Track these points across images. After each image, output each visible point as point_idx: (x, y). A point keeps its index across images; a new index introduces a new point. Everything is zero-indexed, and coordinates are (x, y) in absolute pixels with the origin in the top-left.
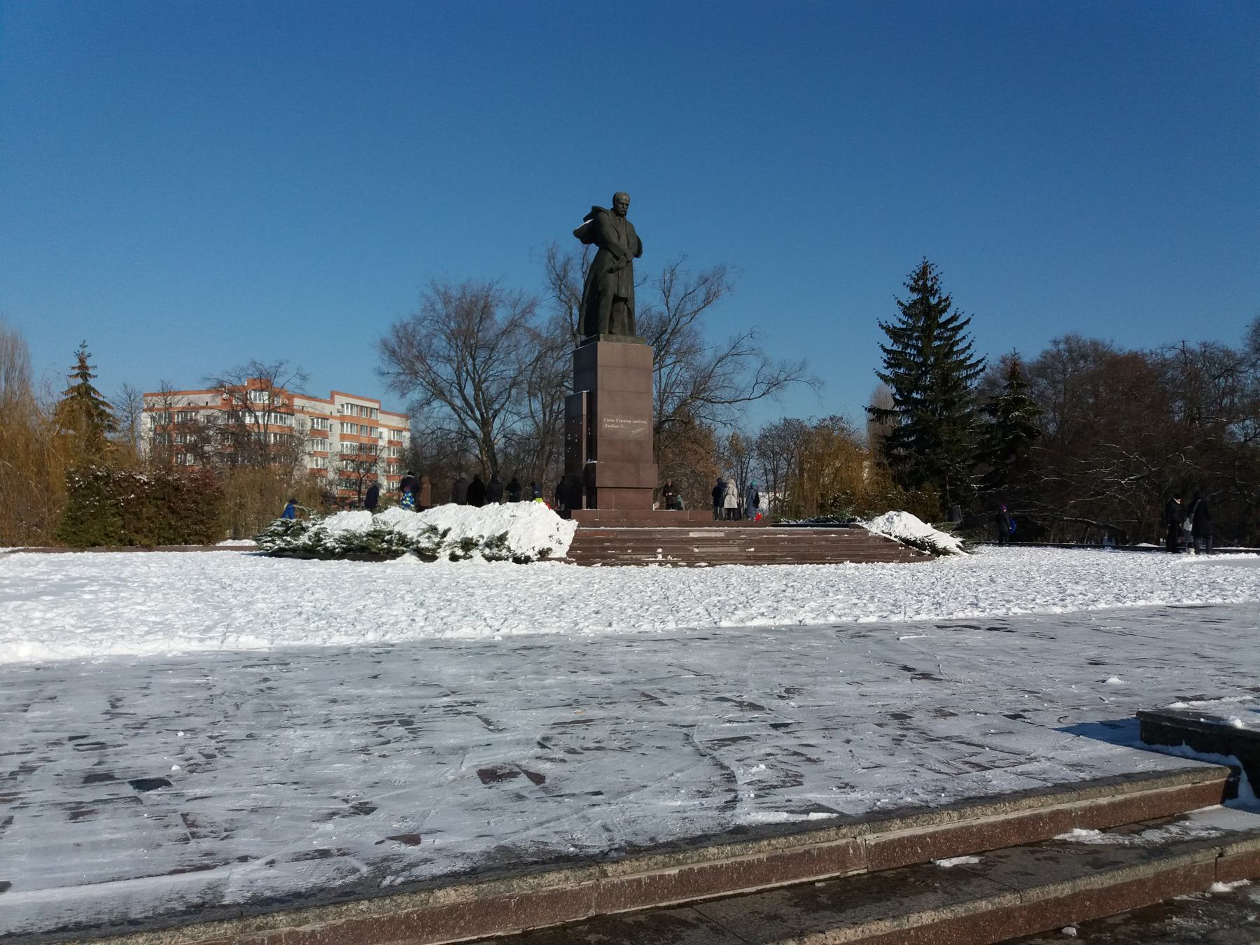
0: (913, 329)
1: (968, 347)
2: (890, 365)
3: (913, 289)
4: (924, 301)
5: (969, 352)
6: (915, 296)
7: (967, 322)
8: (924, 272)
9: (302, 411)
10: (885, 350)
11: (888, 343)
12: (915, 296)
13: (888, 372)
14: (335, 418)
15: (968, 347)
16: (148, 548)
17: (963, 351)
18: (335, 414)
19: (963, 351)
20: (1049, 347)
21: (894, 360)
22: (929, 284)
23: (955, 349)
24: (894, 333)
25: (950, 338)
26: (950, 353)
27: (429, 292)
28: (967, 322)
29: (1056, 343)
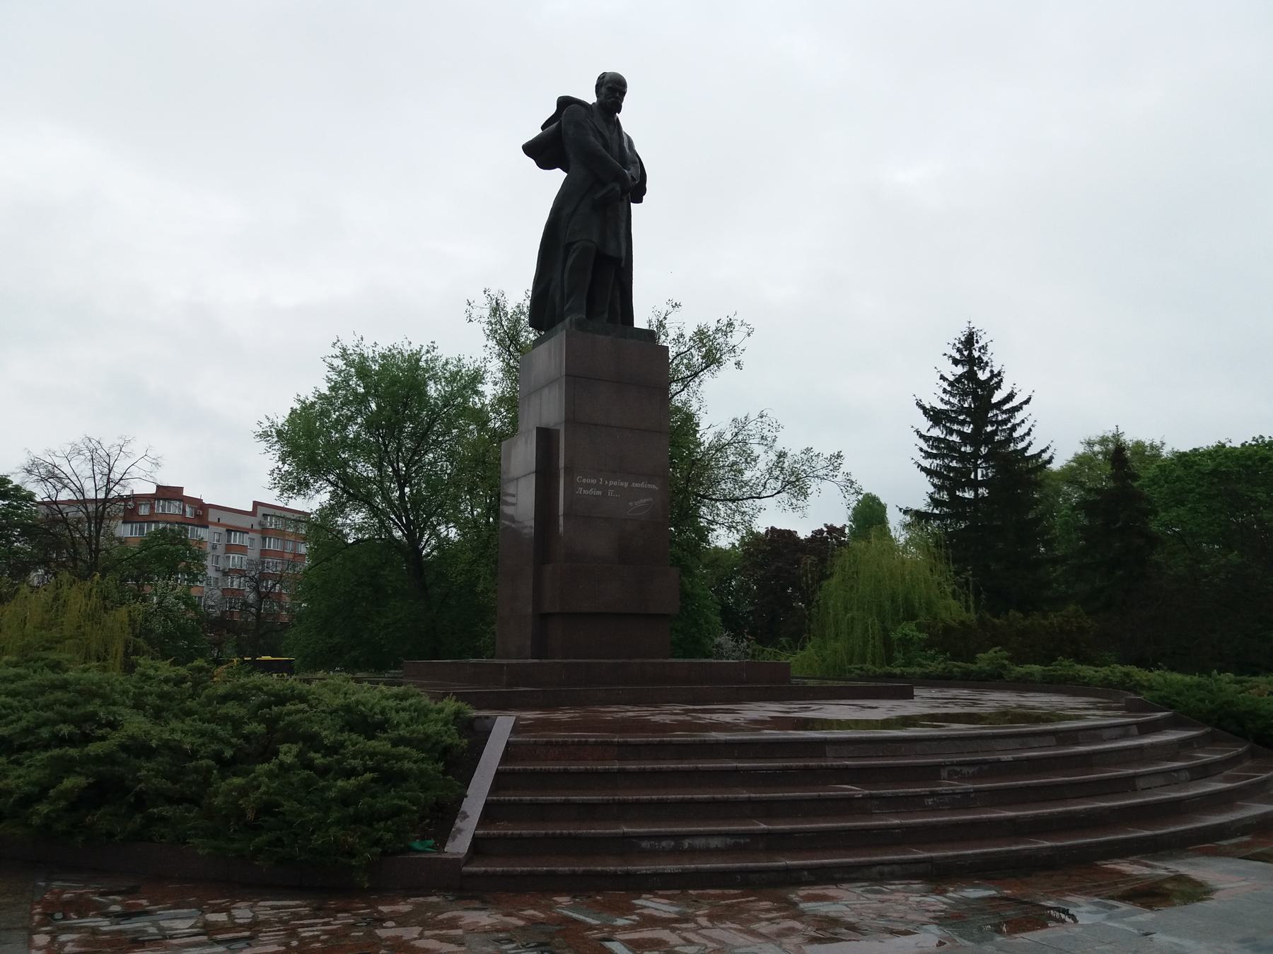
0: (961, 410)
1: (1028, 434)
2: (928, 455)
3: (956, 362)
4: (971, 376)
5: (1027, 439)
6: (960, 370)
7: (1027, 402)
8: (969, 341)
9: (218, 524)
10: (921, 436)
11: (924, 424)
12: (960, 370)
13: (927, 463)
14: (255, 531)
15: (1028, 434)
16: (1220, 452)
17: (1022, 438)
18: (256, 527)
19: (1022, 438)
20: (1081, 450)
21: (938, 448)
22: (976, 354)
23: (1015, 435)
24: (935, 416)
25: (1005, 422)
26: (1010, 439)
27: (339, 363)
28: (1027, 402)
29: (1090, 444)
